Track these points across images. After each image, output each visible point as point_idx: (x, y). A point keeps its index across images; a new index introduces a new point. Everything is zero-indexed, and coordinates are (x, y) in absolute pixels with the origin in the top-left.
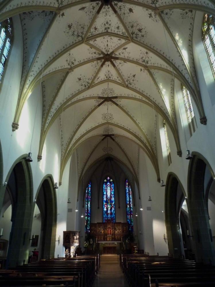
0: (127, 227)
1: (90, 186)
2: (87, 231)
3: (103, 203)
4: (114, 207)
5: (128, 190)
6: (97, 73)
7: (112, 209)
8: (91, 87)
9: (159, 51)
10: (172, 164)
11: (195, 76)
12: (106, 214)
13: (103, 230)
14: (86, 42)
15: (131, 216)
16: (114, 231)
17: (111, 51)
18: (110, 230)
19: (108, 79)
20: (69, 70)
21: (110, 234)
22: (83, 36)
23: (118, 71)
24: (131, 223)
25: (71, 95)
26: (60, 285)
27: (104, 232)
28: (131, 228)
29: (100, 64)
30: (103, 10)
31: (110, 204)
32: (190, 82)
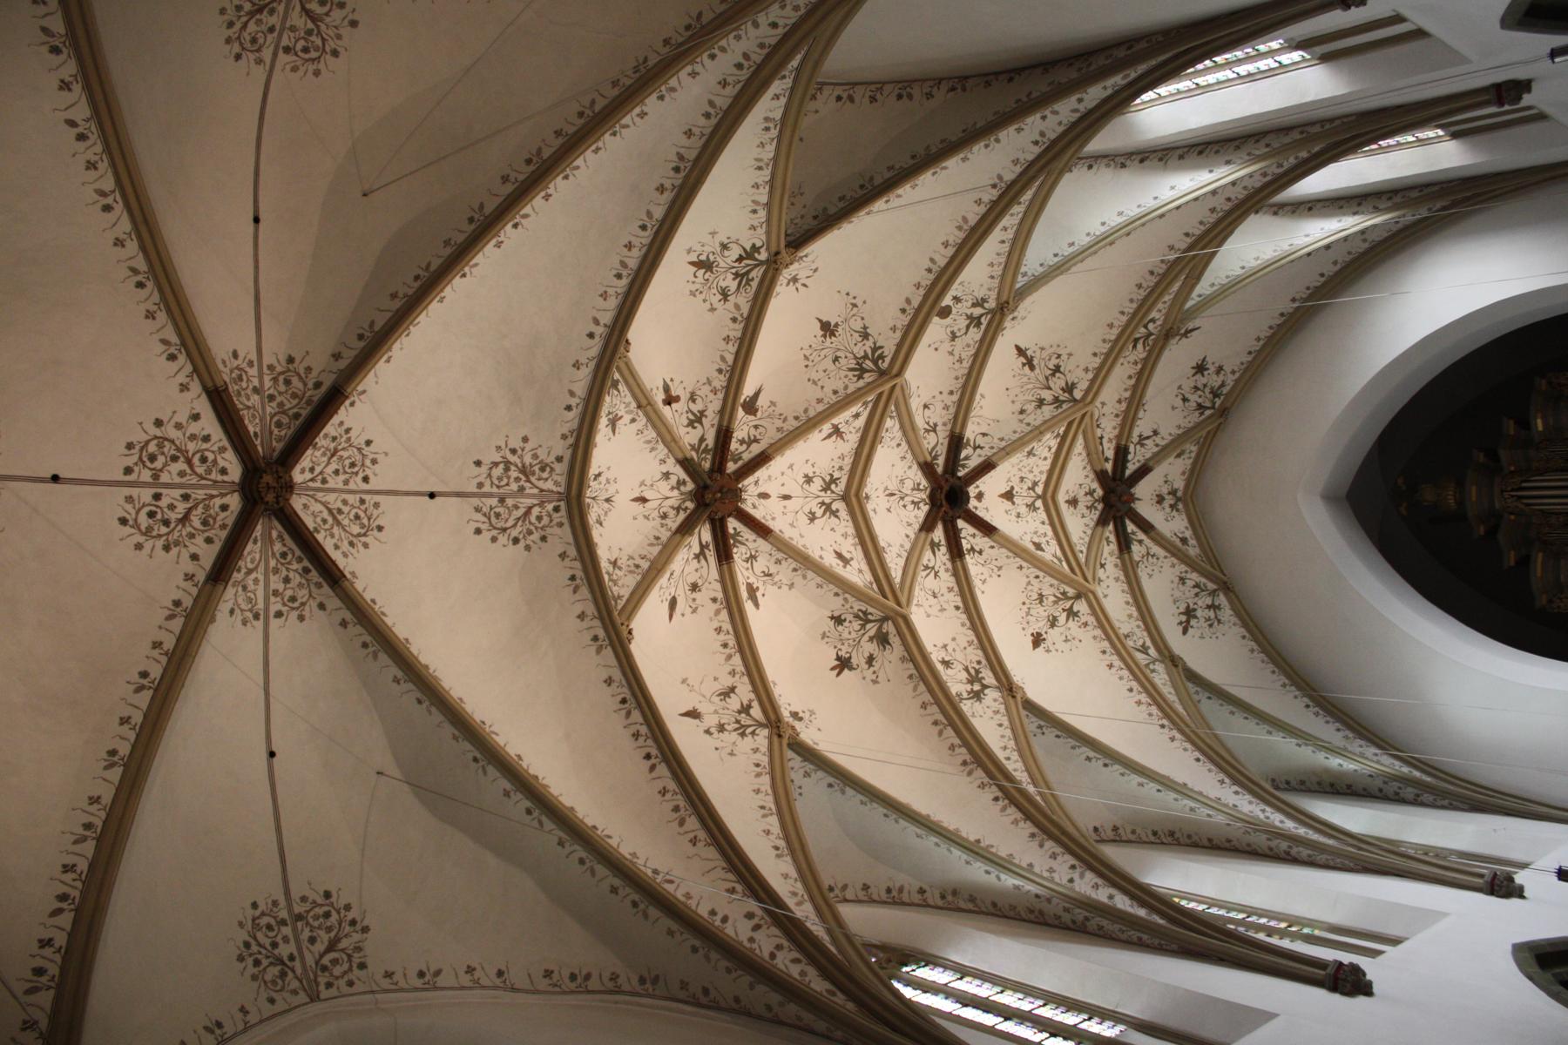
6: (804, 561)
8: (1225, 579)
9: (1143, 293)
10: (1405, 12)
11: (1266, 140)
14: (903, 600)
17: (917, 476)
19: (1039, 497)
20: (780, 736)
22: (876, 613)
23: (1008, 450)
25: (758, 775)
26: (1520, 98)
29: (981, 541)
30: (759, 512)
32: (1280, 166)
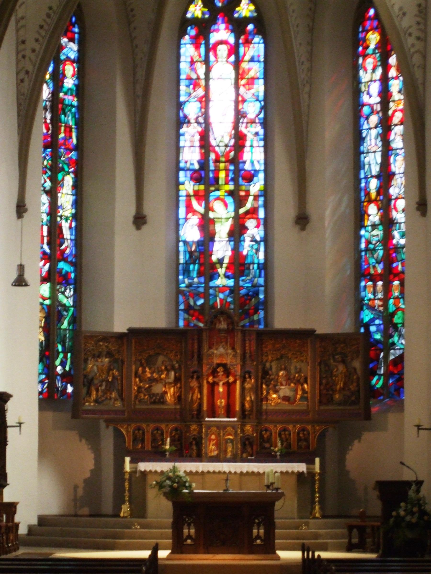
0: (357, 364)
1: (74, 47)
2: (52, 387)
3: (178, 184)
4: (261, 214)
5: (375, 88)
7: (243, 229)
12: (194, 268)
13: (177, 380)
15: (387, 290)
16: (257, 390)
18: (229, 386)
21: (229, 413)
24: (387, 336)
27: (179, 399)
28: (388, 375)
31: (230, 193)
